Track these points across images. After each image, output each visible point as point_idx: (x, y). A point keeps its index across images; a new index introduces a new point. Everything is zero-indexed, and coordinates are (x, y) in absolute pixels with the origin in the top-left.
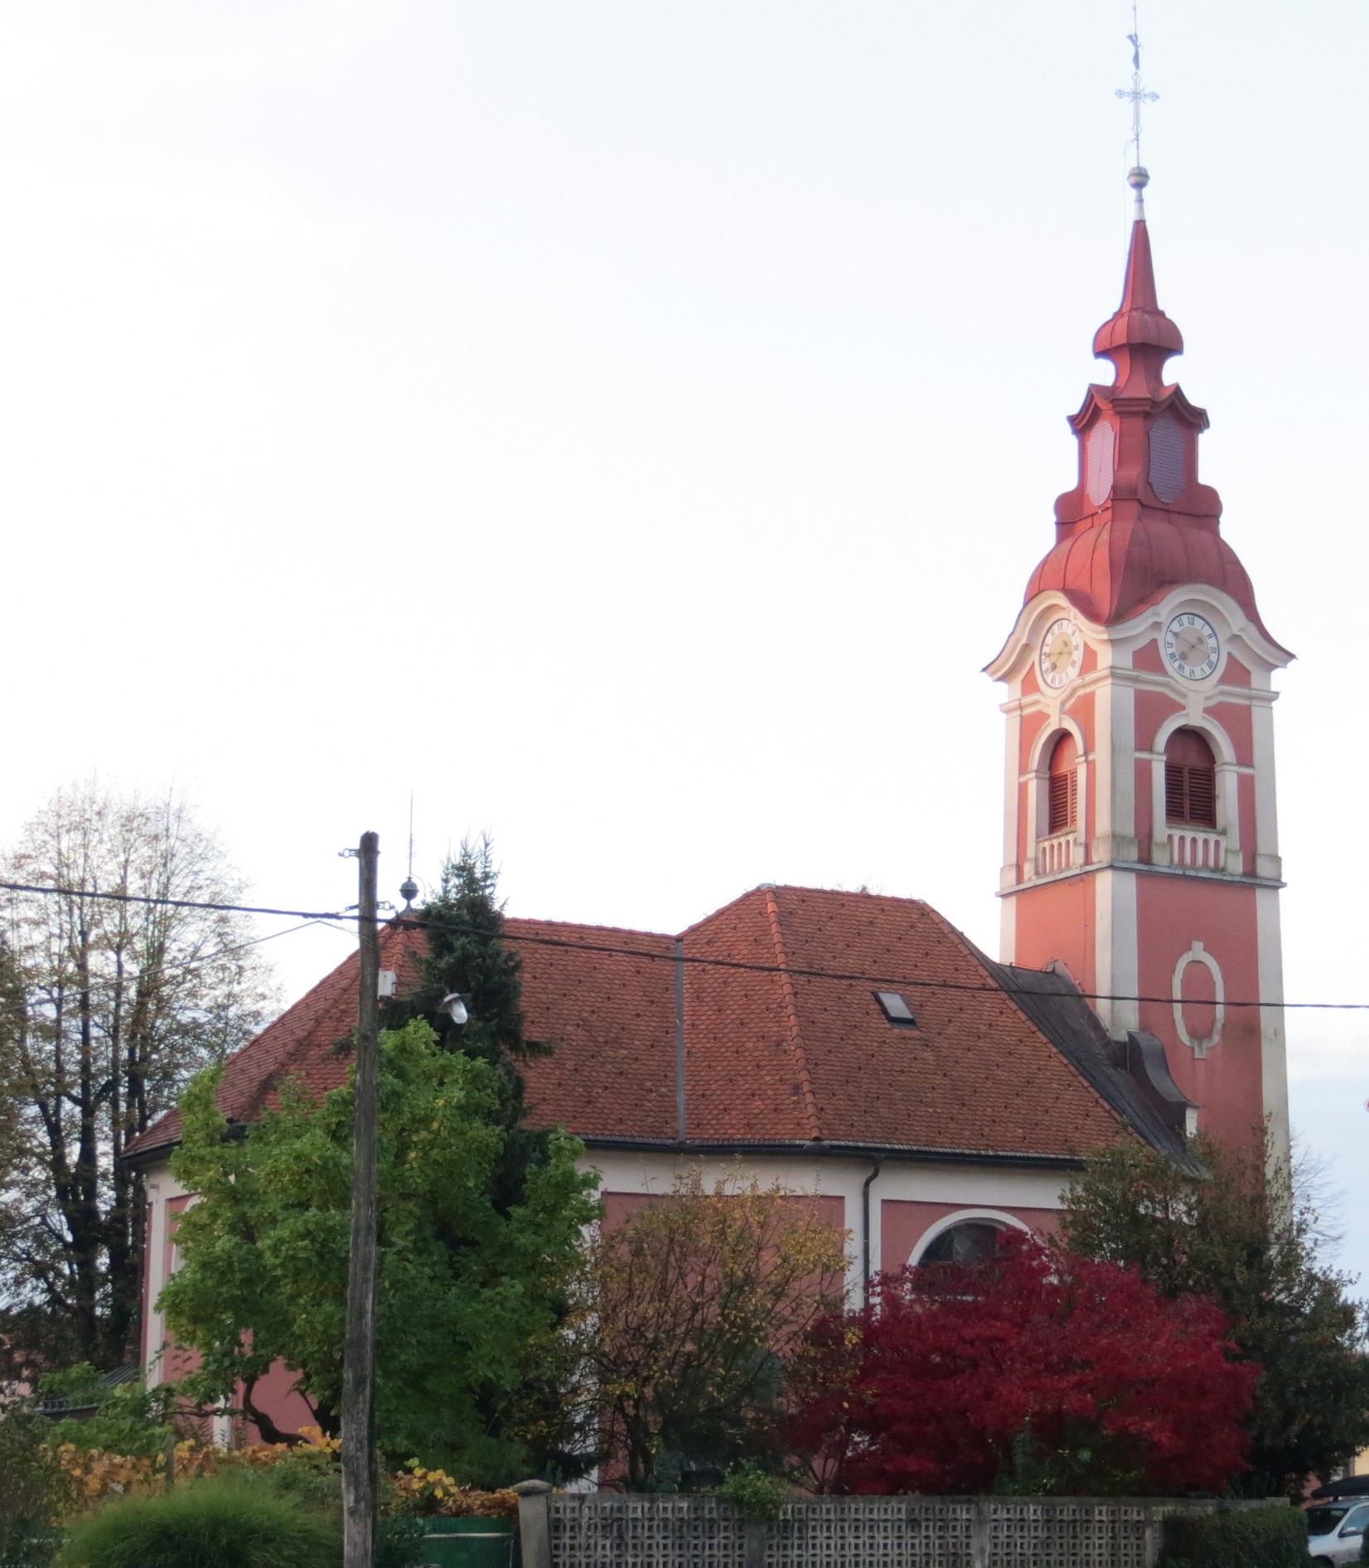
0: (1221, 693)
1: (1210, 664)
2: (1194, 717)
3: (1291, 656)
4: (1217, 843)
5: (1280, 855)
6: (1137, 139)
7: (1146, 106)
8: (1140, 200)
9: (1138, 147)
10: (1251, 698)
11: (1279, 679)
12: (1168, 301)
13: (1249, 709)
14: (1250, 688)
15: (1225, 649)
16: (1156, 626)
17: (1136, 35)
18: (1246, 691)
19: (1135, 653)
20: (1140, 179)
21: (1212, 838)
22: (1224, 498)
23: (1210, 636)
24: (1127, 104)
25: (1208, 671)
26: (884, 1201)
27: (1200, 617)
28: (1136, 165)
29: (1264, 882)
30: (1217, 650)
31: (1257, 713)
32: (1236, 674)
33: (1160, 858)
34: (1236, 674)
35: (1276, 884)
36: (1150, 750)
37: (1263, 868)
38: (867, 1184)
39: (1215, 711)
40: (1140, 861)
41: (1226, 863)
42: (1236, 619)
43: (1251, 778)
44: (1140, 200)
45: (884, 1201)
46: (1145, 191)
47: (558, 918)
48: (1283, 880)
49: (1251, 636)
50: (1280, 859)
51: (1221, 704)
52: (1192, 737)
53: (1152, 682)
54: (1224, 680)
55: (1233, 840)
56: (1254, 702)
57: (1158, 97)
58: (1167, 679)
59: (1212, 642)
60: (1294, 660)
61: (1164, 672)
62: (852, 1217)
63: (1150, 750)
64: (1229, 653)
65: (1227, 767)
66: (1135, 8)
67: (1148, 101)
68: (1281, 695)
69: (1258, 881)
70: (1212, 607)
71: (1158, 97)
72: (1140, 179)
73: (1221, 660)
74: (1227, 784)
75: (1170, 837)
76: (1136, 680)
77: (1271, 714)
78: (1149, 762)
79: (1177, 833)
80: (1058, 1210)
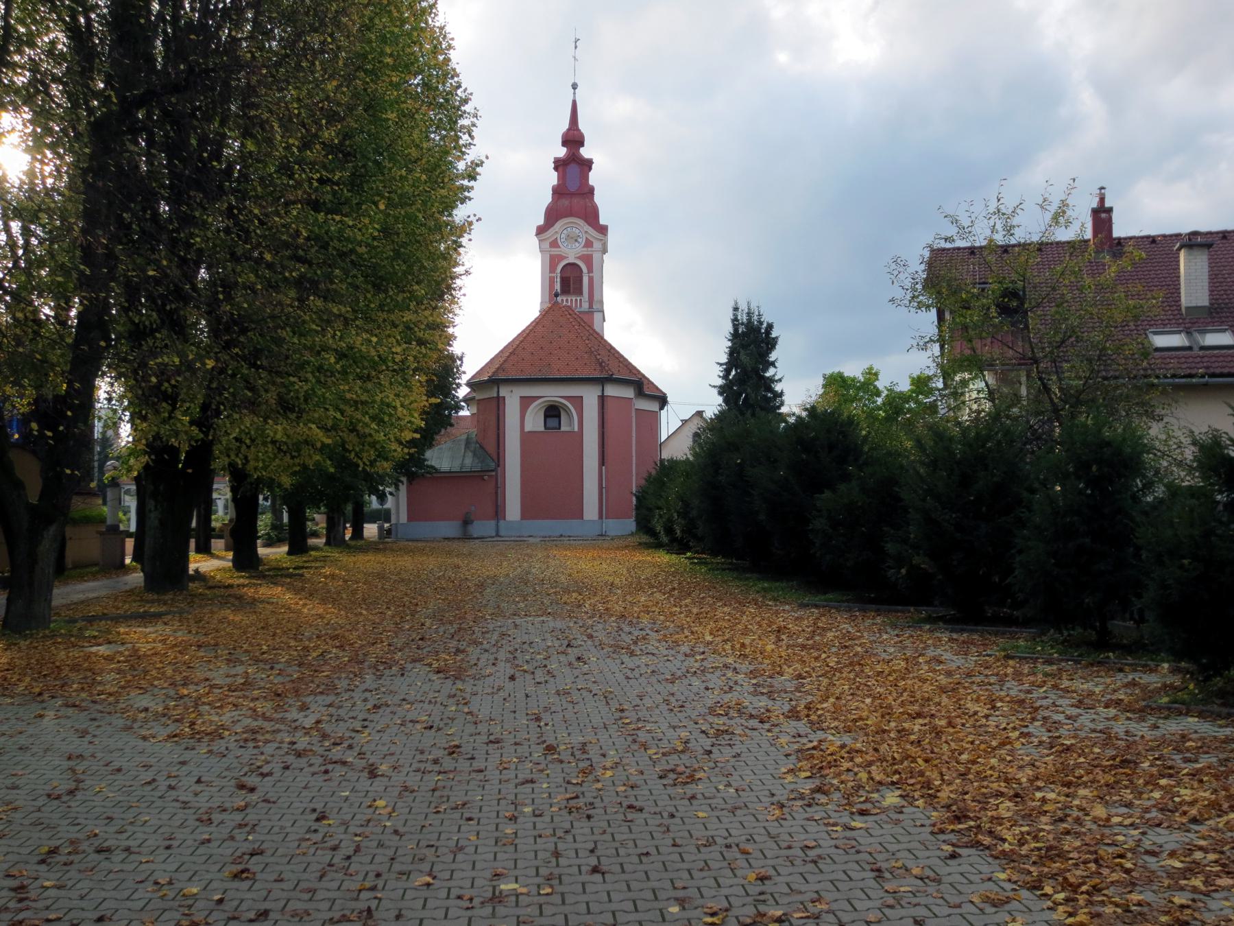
8: (574, 93)
12: (582, 126)
20: (575, 86)
44: (574, 93)
72: (575, 86)
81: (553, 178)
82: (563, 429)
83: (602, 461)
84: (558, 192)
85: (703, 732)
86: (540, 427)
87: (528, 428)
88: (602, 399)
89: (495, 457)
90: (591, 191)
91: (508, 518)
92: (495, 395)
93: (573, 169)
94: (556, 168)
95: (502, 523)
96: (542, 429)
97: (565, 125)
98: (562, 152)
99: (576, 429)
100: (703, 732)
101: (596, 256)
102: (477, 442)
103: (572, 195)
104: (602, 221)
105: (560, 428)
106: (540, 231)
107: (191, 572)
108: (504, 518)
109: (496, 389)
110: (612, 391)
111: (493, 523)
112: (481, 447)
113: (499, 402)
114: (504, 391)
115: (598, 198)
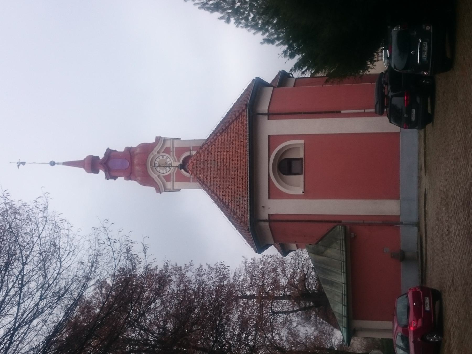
8: (58, 163)
12: (82, 157)
13: (176, 148)
17: (17, 163)
19: (167, 182)
20: (53, 164)
22: (125, 147)
26: (269, 198)
32: (167, 151)
34: (167, 151)
43: (193, 147)
44: (58, 163)
45: (269, 198)
46: (56, 162)
47: (212, 201)
51: (176, 156)
56: (174, 146)
58: (172, 174)
62: (387, 325)
64: (162, 153)
66: (11, 163)
70: (151, 159)
72: (53, 164)
76: (173, 182)
81: (121, 179)
82: (302, 156)
83: (335, 113)
84: (130, 176)
85: (433, 234)
86: (300, 179)
87: (299, 191)
88: (271, 115)
89: (332, 225)
90: (129, 150)
91: (398, 214)
92: (267, 224)
93: (111, 164)
94: (115, 178)
95: (401, 219)
96: (302, 177)
97: (81, 171)
98: (102, 173)
99: (302, 142)
100: (433, 234)
101: (177, 145)
102: (317, 243)
103: (132, 164)
104: (153, 140)
105: (301, 159)
106: (159, 190)
107: (425, 298)
108: (398, 217)
109: (262, 224)
110: (264, 107)
111: (403, 229)
112: (321, 239)
113: (273, 219)
114: (264, 215)
115: (134, 144)
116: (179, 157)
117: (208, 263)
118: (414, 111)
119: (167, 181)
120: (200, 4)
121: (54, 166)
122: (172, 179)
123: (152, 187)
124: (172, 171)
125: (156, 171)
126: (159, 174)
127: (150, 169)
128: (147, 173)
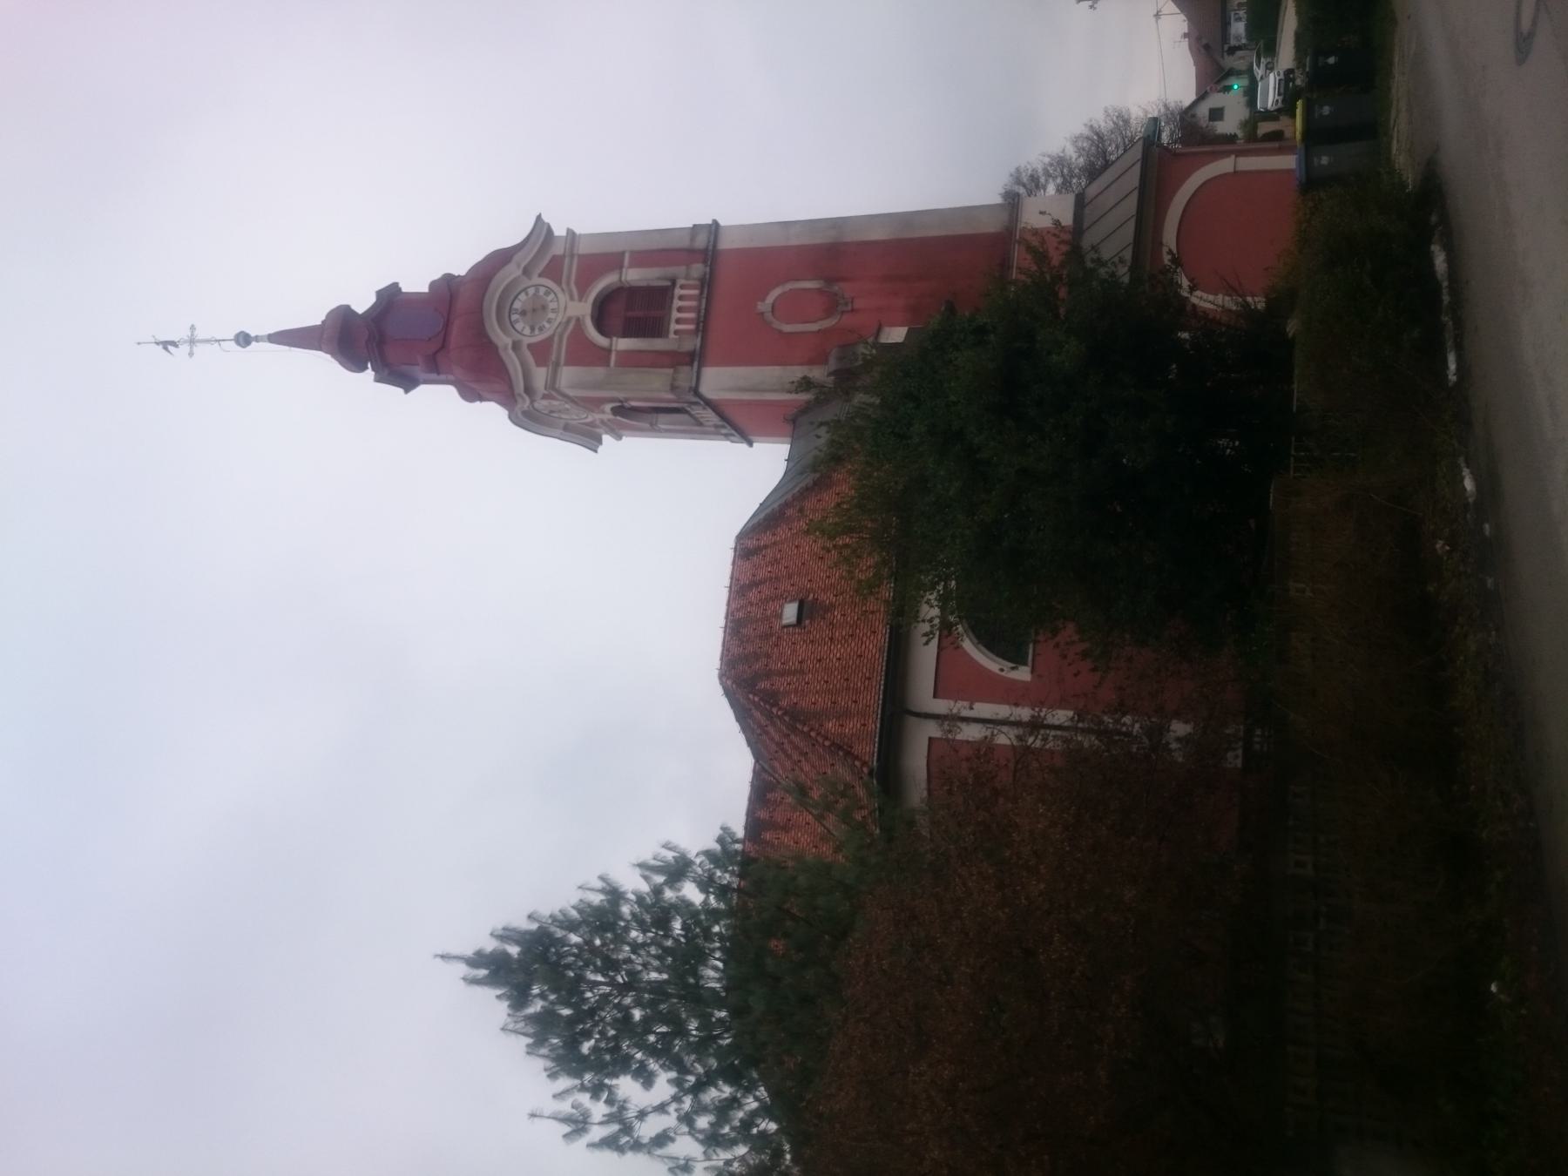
0: (568, 283)
1: (547, 294)
2: (583, 309)
3: (539, 218)
4: (682, 287)
5: (691, 226)
6: (220, 340)
7: (200, 335)
8: (257, 339)
9: (224, 340)
10: (572, 256)
11: (559, 231)
12: (315, 317)
13: (581, 257)
14: (564, 256)
15: (536, 280)
16: (516, 346)
18: (567, 261)
20: (244, 339)
21: (678, 292)
23: (527, 294)
24: (198, 349)
25: (552, 296)
26: (935, 696)
27: (512, 304)
28: (233, 342)
29: (712, 243)
30: (537, 286)
31: (583, 249)
32: (554, 270)
33: (692, 344)
35: (714, 228)
36: (609, 351)
37: (701, 241)
38: (918, 715)
39: (583, 286)
40: (691, 364)
41: (694, 279)
42: (512, 271)
43: (633, 253)
44: (257, 339)
46: (253, 334)
48: (710, 222)
49: (523, 259)
50: (695, 225)
51: (577, 284)
52: (602, 314)
53: (561, 350)
54: (558, 281)
55: (679, 271)
57: (193, 326)
59: (531, 291)
60: (543, 217)
61: (550, 340)
63: (609, 351)
64: (540, 276)
65: (623, 278)
66: (139, 343)
67: (196, 333)
68: (571, 227)
69: (711, 248)
70: (503, 292)
71: (193, 326)
72: (244, 339)
73: (546, 284)
74: (634, 276)
75: (676, 332)
76: (557, 365)
77: (585, 235)
78: (618, 352)
79: (674, 327)
80: (939, 647)
116: (583, 286)
117: (579, 885)
118: (1452, 378)
119: (539, 364)
120: (666, 1160)
121: (249, 348)
122: (553, 357)
123: (509, 246)
124: (559, 330)
125: (514, 331)
126: (519, 337)
127: (499, 331)
128: (486, 336)
